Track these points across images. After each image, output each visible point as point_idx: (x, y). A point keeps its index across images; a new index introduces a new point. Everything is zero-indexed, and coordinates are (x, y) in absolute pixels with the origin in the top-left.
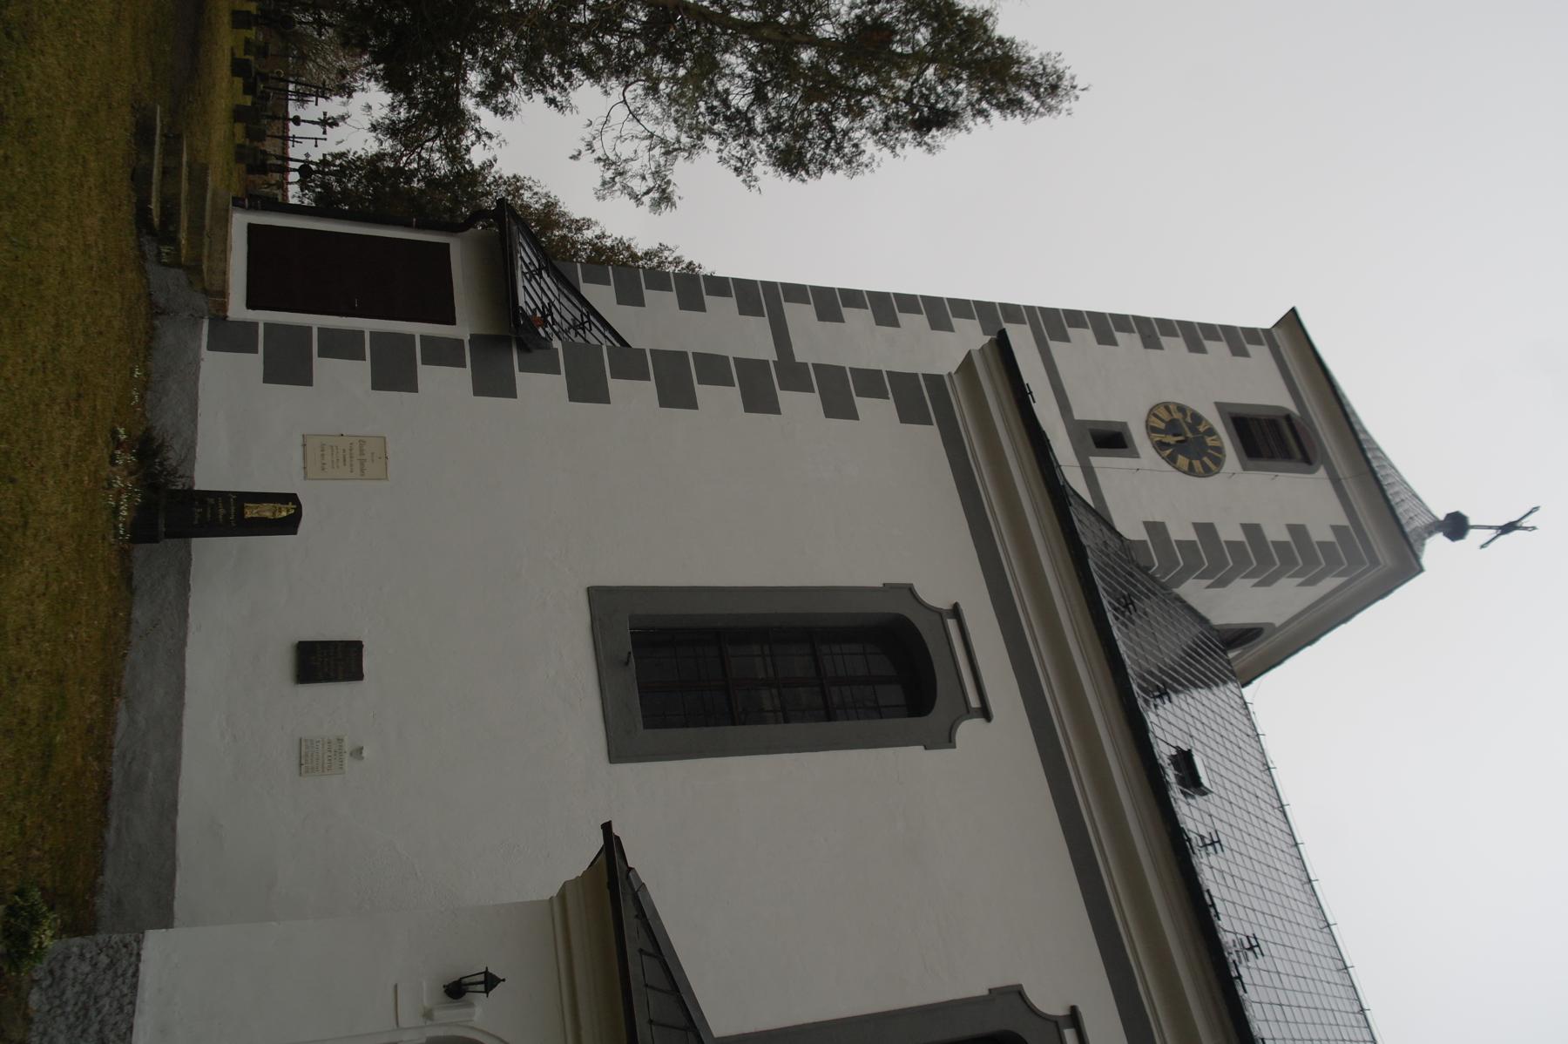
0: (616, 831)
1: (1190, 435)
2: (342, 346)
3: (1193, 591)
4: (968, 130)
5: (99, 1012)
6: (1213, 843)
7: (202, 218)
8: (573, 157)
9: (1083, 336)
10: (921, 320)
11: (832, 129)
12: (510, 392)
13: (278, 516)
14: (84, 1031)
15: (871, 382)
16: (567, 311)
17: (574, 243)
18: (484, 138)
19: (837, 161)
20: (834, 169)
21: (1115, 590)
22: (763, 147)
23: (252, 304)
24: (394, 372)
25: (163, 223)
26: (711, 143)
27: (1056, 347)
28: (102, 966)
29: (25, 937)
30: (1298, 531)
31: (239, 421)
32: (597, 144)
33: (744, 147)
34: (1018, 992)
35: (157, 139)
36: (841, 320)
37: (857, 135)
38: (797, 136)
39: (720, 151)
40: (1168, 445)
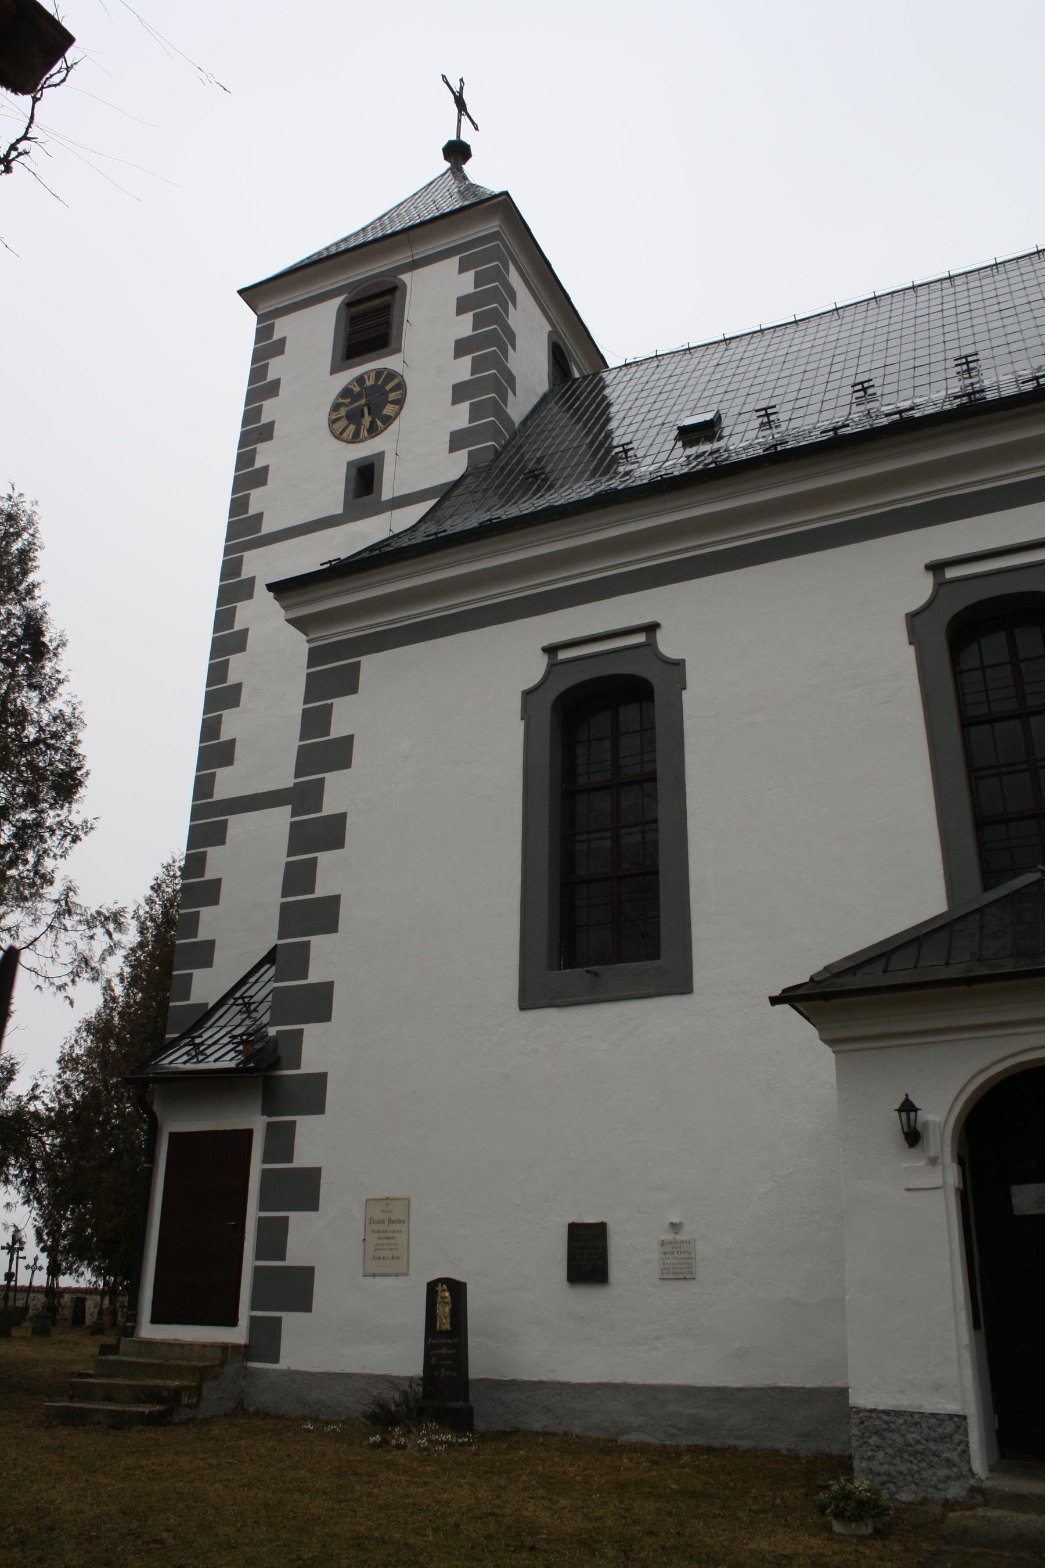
0: (777, 992)
1: (363, 401)
2: (274, 1239)
3: (518, 408)
4: (43, 606)
5: (919, 1442)
6: (768, 415)
7: (152, 1365)
8: (72, 1003)
9: (258, 499)
10: (235, 661)
11: (37, 741)
12: (320, 1079)
13: (449, 1300)
14: (934, 1454)
15: (315, 721)
16: (232, 1019)
17: (127, 1005)
18: (37, 1093)
19: (69, 738)
20: (76, 742)
21: (520, 486)
22: (52, 813)
23: (233, 1322)
24: (302, 1189)
25: (161, 1401)
26: (49, 864)
27: (268, 527)
28: (879, 1442)
29: (861, 1503)
30: (463, 305)
31: (353, 1332)
32: (58, 982)
33: (52, 832)
34: (913, 618)
35: (78, 1405)
36: (233, 742)
37: (46, 718)
38: (44, 779)
39: (55, 856)
40: (373, 423)
